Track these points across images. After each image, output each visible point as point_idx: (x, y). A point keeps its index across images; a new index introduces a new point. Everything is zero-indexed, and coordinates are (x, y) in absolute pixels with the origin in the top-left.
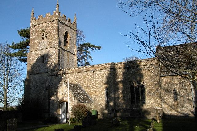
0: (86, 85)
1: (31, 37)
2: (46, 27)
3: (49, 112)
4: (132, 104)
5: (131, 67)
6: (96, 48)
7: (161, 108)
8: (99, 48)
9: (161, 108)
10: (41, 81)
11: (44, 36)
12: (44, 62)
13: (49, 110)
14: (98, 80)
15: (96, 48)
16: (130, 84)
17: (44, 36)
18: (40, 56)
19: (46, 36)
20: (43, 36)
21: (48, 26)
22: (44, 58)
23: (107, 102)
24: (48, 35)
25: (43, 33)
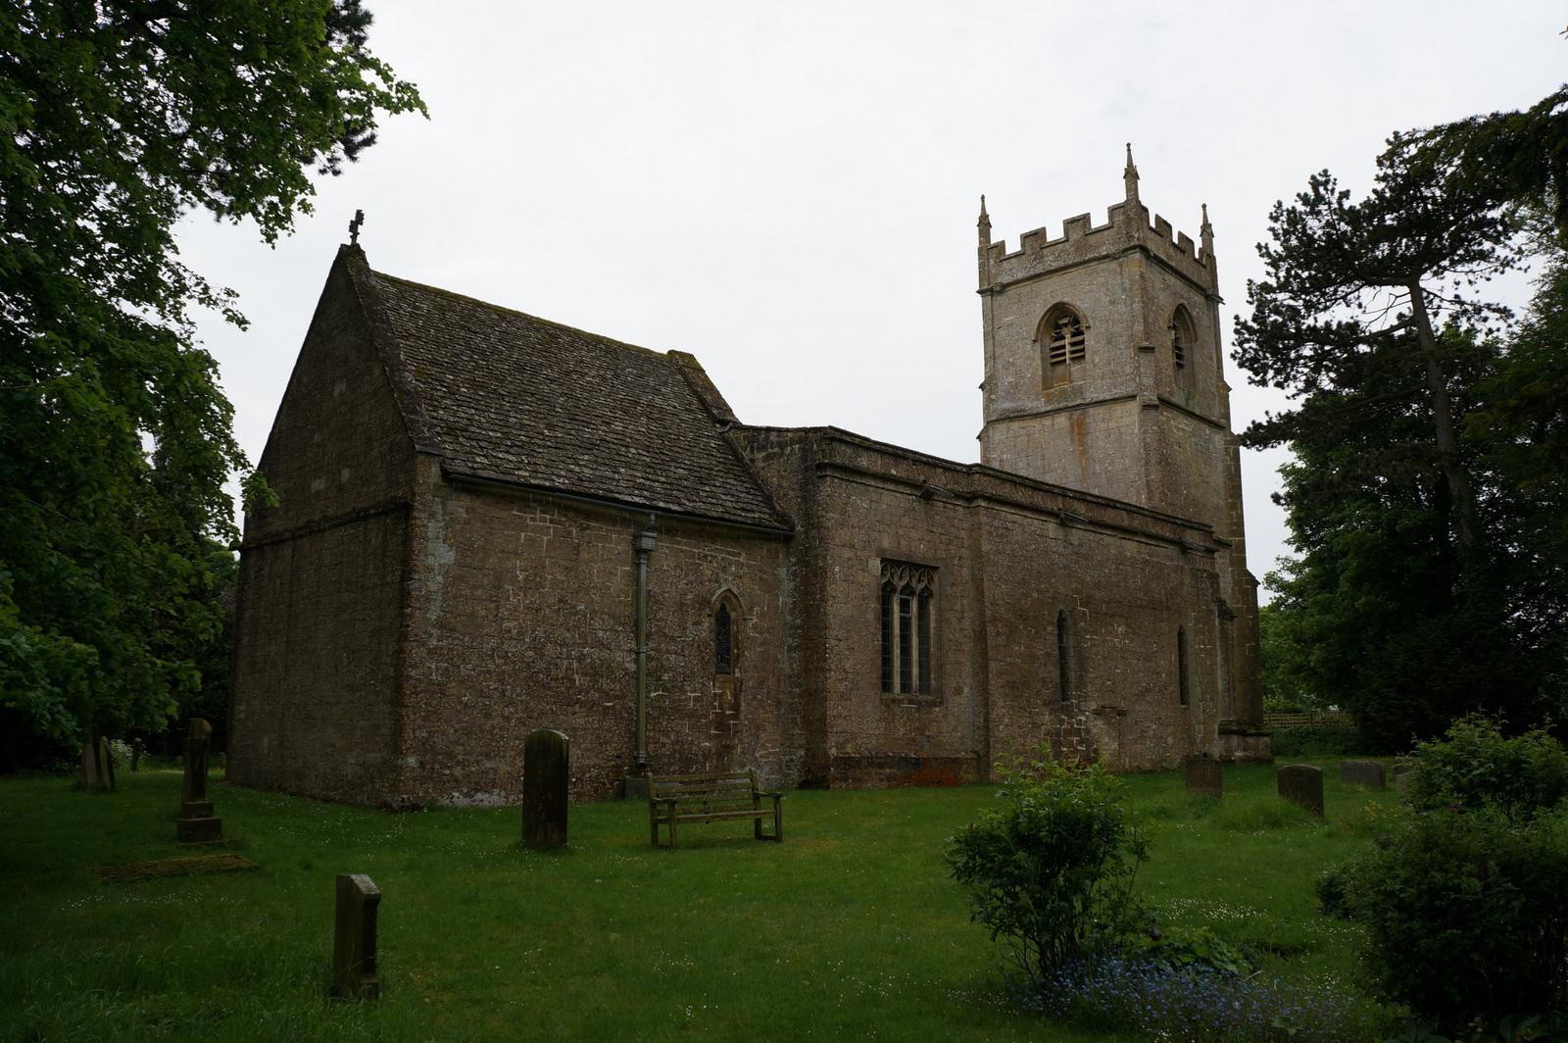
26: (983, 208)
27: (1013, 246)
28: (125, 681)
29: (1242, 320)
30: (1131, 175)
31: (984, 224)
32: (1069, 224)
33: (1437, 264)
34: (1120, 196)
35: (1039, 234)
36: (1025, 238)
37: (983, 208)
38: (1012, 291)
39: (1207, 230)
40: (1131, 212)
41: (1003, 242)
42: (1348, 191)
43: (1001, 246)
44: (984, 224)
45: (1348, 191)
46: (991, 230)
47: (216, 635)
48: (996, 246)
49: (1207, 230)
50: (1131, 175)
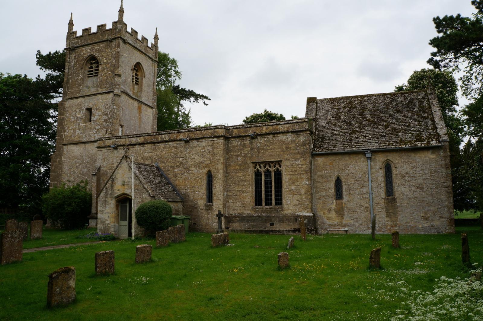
0: (171, 167)
1: (66, 71)
2: (96, 51)
3: (96, 218)
4: (256, 205)
5: (258, 135)
6: (197, 97)
7: (312, 215)
8: (210, 99)
9: (312, 215)
10: (84, 158)
11: (92, 70)
12: (90, 121)
13: (97, 214)
14: (194, 158)
15: (197, 97)
16: (255, 168)
17: (92, 70)
18: (458, 100)
19: (92, 71)
20: (90, 68)
21: (99, 51)
22: (91, 112)
23: (96, 268)
24: (100, 68)
25: (92, 64)
26: (122, 5)
27: (79, 34)
28: (305, 317)
29: (465, 97)
30: (121, 12)
31: (71, 24)
32: (84, 30)
33: (481, 96)
34: (116, 19)
35: (104, 26)
36: (98, 27)
37: (122, 5)
38: (127, 46)
39: (156, 38)
40: (120, 24)
41: (76, 31)
42: (25, 75)
43: (75, 33)
44: (71, 24)
45: (25, 75)
46: (124, 14)
47: (290, 194)
48: (73, 33)
49: (156, 38)
50: (121, 12)
